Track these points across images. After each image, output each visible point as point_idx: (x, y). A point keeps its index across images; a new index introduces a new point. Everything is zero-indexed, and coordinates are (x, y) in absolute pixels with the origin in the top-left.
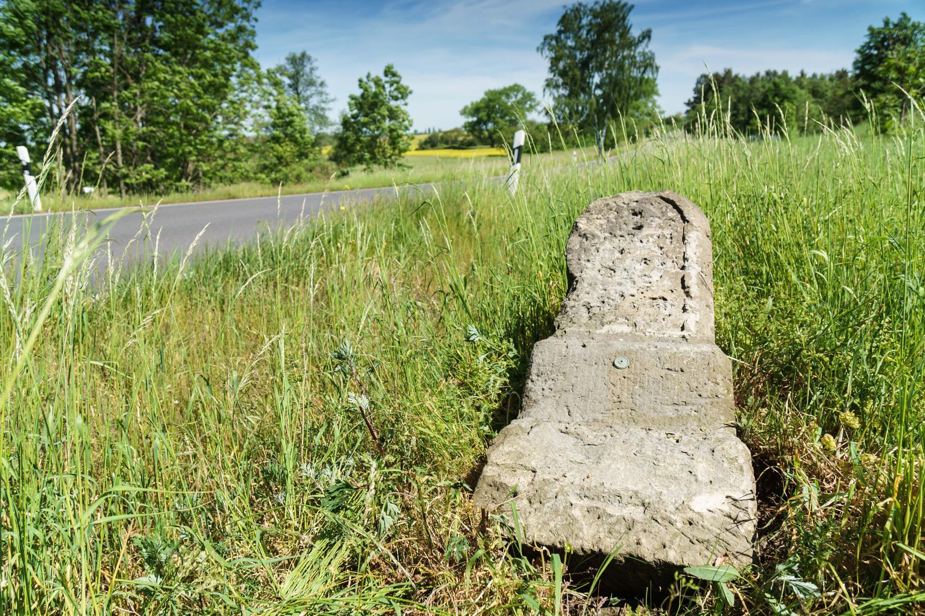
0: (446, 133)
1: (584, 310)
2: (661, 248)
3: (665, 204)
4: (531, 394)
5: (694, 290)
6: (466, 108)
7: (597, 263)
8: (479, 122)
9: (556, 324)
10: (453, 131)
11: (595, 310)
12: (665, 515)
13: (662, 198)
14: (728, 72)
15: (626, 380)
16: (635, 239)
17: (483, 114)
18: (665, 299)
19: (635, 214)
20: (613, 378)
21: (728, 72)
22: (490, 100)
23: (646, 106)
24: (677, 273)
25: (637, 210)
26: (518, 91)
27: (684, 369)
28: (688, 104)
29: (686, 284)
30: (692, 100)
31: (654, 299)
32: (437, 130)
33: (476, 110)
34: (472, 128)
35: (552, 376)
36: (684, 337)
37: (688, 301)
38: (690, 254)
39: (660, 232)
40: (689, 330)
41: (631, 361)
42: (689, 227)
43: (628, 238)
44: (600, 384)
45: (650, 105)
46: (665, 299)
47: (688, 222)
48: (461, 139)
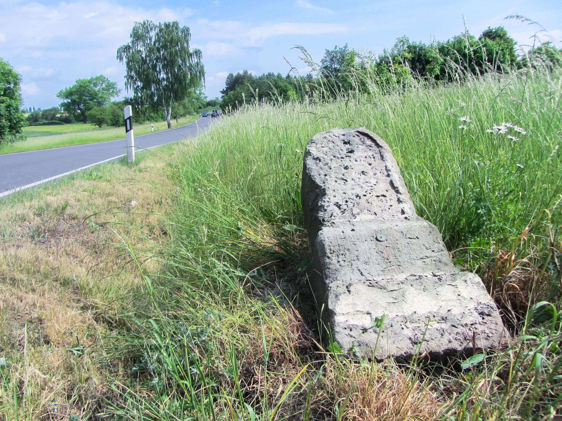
0: (46, 111)
1: (336, 209)
2: (370, 164)
3: (361, 136)
4: (331, 266)
5: (401, 189)
6: (61, 92)
7: (333, 176)
8: (74, 102)
9: (321, 219)
10: (51, 110)
11: (344, 207)
12: (458, 322)
13: (358, 132)
14: (246, 72)
15: (388, 248)
16: (352, 159)
17: (75, 97)
18: (384, 196)
19: (345, 143)
20: (381, 248)
21: (246, 72)
22: (81, 86)
23: (195, 93)
24: (386, 180)
25: (346, 140)
26: (103, 82)
27: (419, 237)
28: (223, 92)
29: (395, 185)
30: (225, 89)
31: (378, 196)
32: (36, 109)
33: (69, 94)
34: (67, 107)
35: (341, 252)
36: (406, 218)
37: (399, 196)
38: (390, 167)
39: (365, 154)
40: (407, 213)
41: (387, 236)
42: (383, 150)
43: (347, 159)
44: (373, 252)
45: (198, 92)
46: (384, 196)
47: (381, 147)
48: (58, 115)
